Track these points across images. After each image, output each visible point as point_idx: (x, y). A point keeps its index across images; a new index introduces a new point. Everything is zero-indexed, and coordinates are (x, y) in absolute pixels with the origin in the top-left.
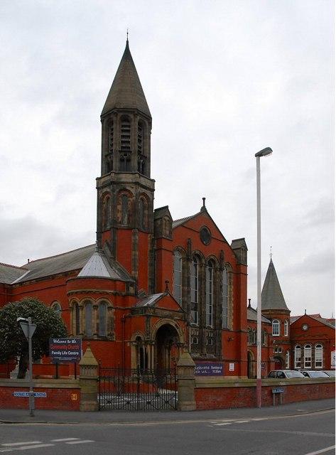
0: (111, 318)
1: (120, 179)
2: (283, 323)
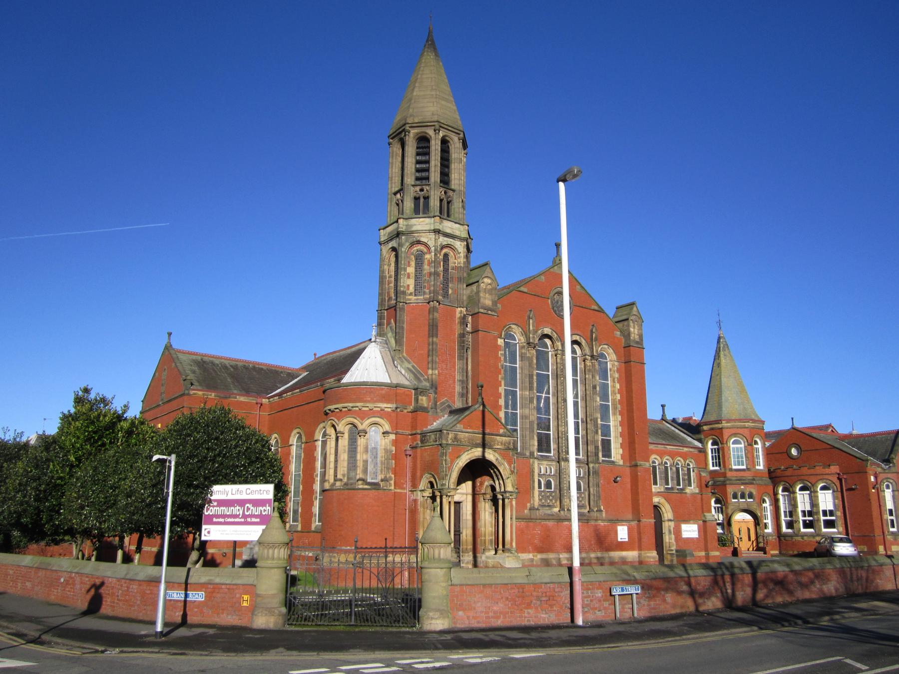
0: (386, 450)
1: (412, 226)
2: (750, 445)
